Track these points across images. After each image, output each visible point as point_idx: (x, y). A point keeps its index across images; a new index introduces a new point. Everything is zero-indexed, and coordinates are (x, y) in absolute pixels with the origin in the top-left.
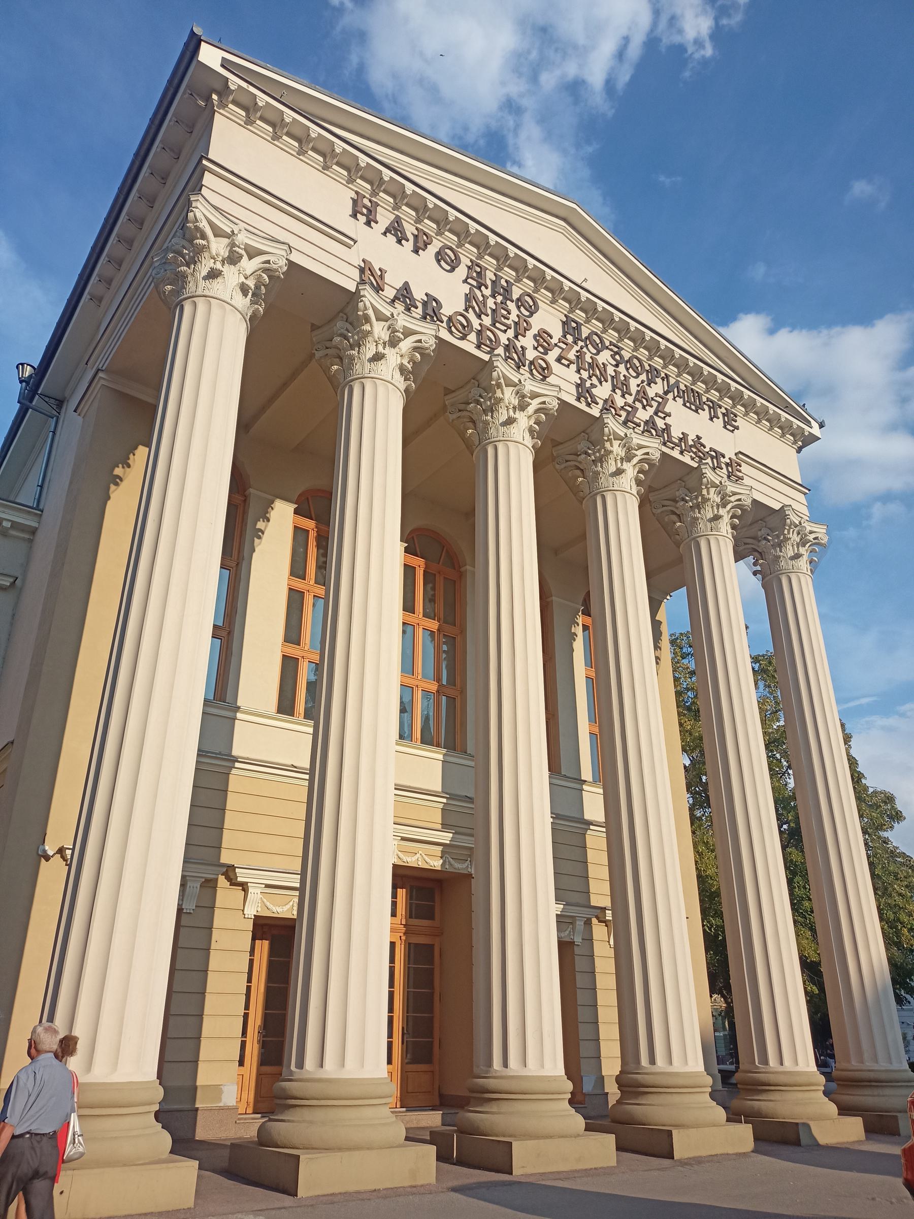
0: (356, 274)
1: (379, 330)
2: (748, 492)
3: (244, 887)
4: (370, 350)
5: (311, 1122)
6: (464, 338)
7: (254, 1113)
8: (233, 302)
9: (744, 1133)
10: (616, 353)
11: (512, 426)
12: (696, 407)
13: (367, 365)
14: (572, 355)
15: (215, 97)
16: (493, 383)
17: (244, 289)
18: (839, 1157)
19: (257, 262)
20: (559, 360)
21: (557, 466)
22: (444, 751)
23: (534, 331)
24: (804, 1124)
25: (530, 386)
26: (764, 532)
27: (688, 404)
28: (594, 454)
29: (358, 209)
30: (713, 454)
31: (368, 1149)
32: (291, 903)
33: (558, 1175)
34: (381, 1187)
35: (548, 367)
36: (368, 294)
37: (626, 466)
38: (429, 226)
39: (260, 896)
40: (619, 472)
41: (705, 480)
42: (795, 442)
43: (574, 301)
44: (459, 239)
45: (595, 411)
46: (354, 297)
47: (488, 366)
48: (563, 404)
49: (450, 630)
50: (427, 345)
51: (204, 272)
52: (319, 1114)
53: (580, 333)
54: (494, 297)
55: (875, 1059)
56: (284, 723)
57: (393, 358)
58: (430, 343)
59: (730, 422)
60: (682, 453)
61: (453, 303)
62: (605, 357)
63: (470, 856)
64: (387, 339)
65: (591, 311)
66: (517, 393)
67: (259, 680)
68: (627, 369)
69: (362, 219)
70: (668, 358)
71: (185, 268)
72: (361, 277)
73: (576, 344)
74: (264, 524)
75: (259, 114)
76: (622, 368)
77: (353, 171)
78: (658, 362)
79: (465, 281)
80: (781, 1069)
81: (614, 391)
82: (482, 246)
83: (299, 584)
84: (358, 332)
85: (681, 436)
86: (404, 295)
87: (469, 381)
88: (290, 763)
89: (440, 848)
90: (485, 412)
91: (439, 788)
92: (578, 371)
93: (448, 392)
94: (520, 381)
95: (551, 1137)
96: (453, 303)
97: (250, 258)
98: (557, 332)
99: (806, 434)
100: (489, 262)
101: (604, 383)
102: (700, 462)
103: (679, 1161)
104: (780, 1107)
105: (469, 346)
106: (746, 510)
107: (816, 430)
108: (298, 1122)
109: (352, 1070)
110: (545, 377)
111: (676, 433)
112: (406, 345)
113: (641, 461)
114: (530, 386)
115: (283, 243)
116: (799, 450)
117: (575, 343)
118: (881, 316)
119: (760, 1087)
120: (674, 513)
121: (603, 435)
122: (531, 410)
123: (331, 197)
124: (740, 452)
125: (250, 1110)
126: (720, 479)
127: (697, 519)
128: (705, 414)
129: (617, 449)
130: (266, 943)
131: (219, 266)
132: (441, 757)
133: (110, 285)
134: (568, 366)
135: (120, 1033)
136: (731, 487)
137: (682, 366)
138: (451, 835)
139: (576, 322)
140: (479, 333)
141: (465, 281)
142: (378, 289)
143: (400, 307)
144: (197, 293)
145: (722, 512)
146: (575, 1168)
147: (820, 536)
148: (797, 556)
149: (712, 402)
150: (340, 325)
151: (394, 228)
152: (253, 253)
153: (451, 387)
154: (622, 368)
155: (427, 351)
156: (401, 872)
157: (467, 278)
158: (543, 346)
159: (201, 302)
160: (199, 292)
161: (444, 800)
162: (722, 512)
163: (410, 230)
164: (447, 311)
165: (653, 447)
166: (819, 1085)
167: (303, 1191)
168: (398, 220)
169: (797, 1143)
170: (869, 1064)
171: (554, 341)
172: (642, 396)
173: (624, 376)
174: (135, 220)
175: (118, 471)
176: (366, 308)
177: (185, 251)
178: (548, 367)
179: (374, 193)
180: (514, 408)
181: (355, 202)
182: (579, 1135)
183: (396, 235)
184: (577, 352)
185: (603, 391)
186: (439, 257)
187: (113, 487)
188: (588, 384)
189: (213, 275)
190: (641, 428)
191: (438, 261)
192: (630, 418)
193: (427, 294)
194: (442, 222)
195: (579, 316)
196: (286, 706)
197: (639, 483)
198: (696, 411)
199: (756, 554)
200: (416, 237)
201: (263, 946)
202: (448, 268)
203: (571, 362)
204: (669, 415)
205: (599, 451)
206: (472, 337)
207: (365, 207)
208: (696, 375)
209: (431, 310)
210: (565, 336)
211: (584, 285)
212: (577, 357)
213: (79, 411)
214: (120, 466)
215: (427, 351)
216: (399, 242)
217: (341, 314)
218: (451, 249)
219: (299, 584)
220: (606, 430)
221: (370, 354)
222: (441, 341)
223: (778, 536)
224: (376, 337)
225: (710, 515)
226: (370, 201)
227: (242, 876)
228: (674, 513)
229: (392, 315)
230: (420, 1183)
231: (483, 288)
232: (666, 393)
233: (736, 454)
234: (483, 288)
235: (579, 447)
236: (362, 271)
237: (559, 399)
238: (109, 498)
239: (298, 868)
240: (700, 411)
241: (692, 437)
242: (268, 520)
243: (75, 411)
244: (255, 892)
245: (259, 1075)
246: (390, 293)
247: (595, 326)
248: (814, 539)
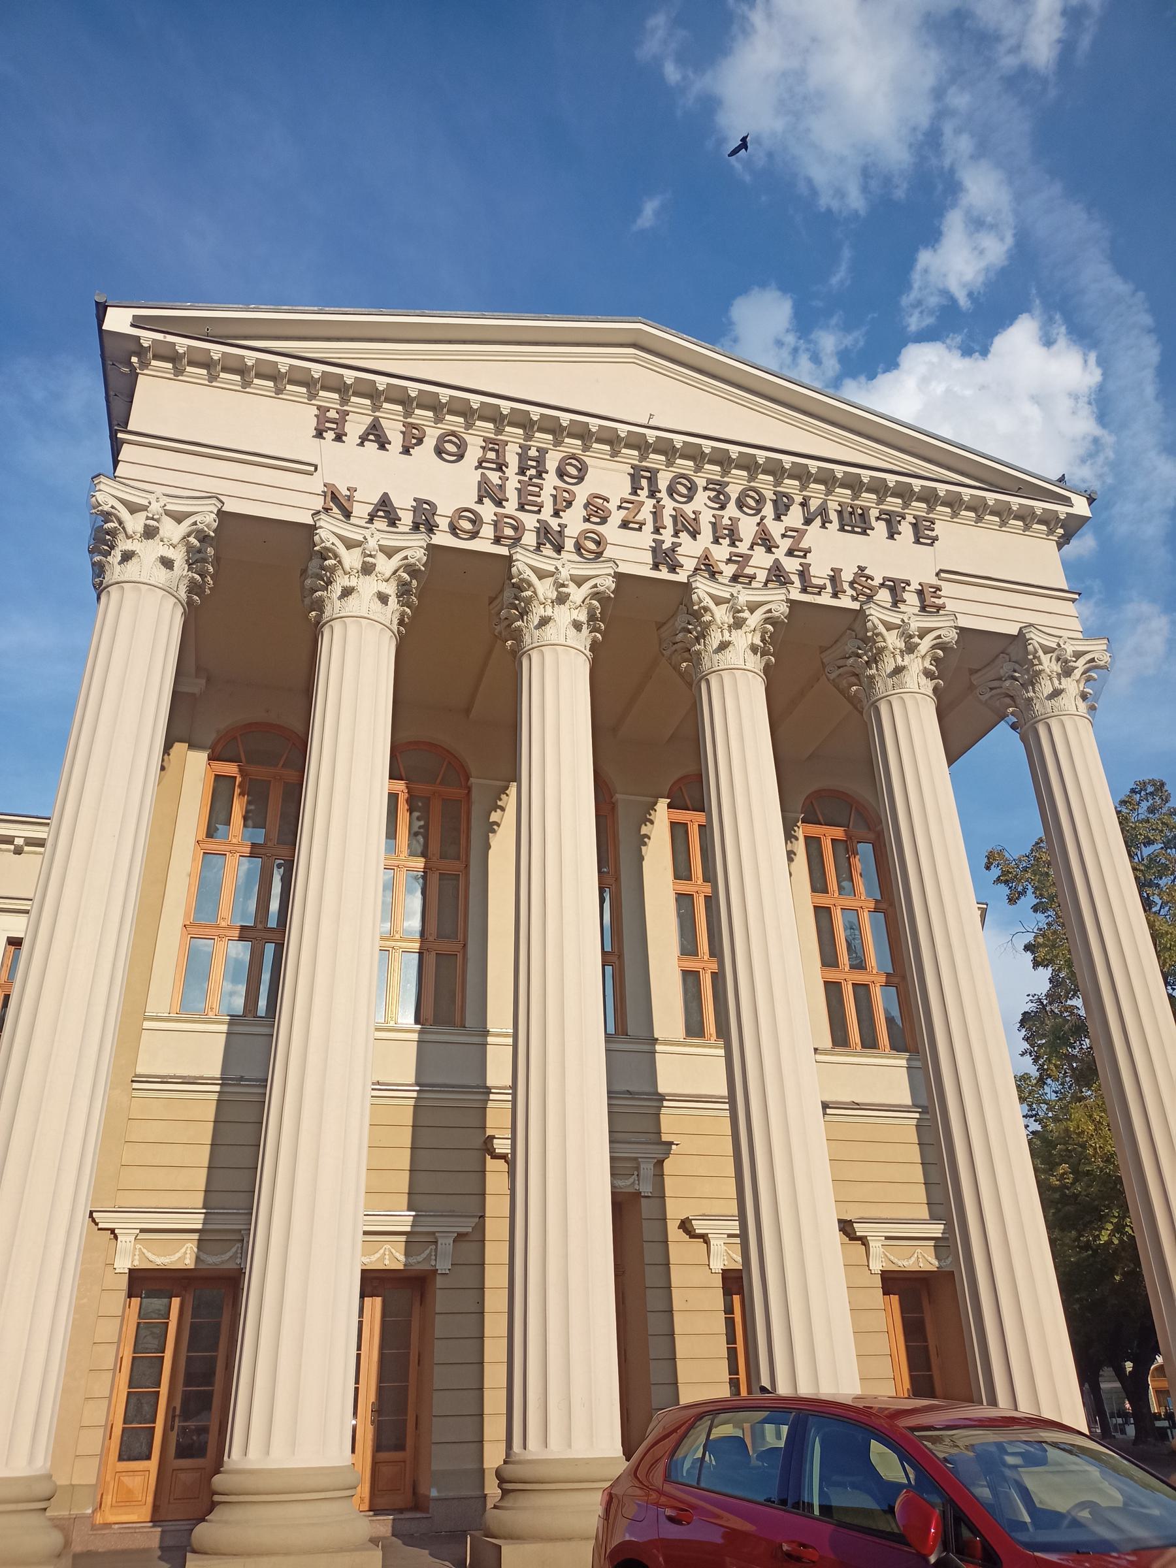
3: (705, 1238)
4: (715, 638)
6: (474, 535)
8: (922, 691)
10: (719, 493)
15: (134, 359)
19: (759, 614)
32: (382, 1251)
58: (782, 610)
59: (923, 534)
64: (731, 621)
66: (1058, 659)
67: (668, 1014)
69: (330, 435)
75: (383, 398)
77: (310, 385)
90: (697, 639)
91: (907, 1100)
94: (903, 621)
109: (581, 1450)
116: (1060, 546)
121: (1028, 653)
123: (284, 422)
124: (942, 571)
130: (378, 1301)
132: (904, 1063)
134: (640, 529)
143: (548, 550)
161: (917, 1115)
189: (724, 646)
198: (864, 533)
201: (375, 1305)
211: (652, 423)
221: (889, 669)
222: (793, 603)
223: (1027, 671)
227: (699, 1227)
237: (956, 628)
239: (735, 1211)
244: (875, 1246)
245: (375, 1464)
247: (571, 446)
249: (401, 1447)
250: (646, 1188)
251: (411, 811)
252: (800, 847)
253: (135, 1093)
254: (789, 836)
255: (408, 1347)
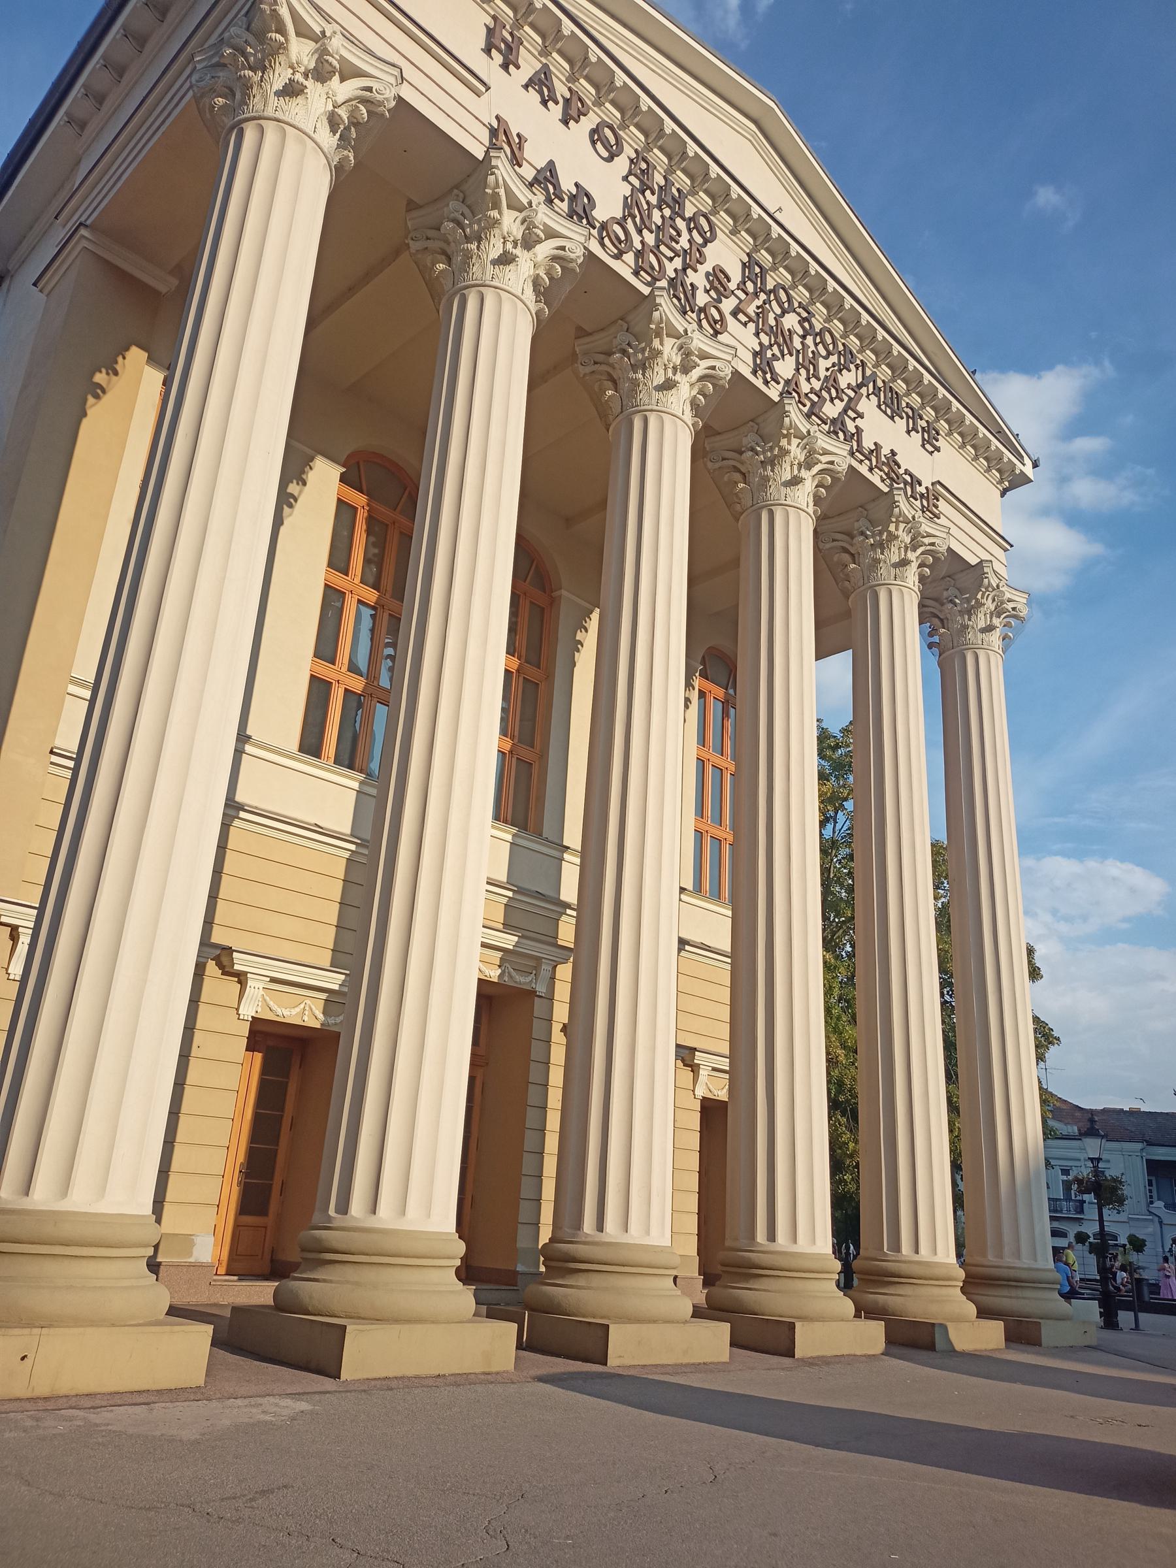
0: (485, 136)
1: (510, 222)
2: (944, 535)
3: (241, 978)
4: (495, 249)
5: (357, 1284)
6: (618, 256)
7: (227, 1274)
9: (873, 1334)
11: (671, 392)
12: (893, 411)
13: (490, 267)
14: (751, 310)
16: (653, 326)
17: (333, 121)
18: (976, 1363)
19: (351, 88)
20: (734, 314)
21: (710, 465)
22: (514, 830)
23: (707, 267)
24: (941, 1325)
25: (699, 341)
26: (952, 591)
27: (883, 407)
28: (764, 452)
29: (496, 41)
30: (908, 478)
31: (433, 1322)
32: (302, 1006)
33: (679, 1368)
34: (446, 1372)
35: (722, 320)
36: (502, 166)
37: (804, 474)
38: (586, 89)
39: (262, 992)
40: (795, 481)
41: (896, 510)
42: (1001, 482)
43: (761, 236)
44: (623, 117)
45: (773, 392)
46: (484, 166)
47: (649, 302)
48: (736, 374)
49: (533, 673)
50: (572, 256)
51: (278, 85)
52: (369, 1274)
53: (763, 282)
54: (661, 210)
55: (1018, 1254)
56: (307, 766)
57: (526, 266)
58: (578, 254)
59: (930, 440)
60: (871, 470)
61: (607, 208)
62: (791, 321)
63: (535, 968)
64: (519, 237)
65: (781, 254)
66: (680, 348)
68: (816, 345)
70: (868, 339)
71: (251, 73)
72: (491, 141)
73: (758, 297)
74: (298, 488)
76: (809, 340)
78: (854, 342)
79: (625, 178)
80: (916, 1258)
81: (797, 370)
82: (653, 133)
83: (339, 581)
84: (480, 220)
85: (873, 447)
86: (547, 178)
87: (615, 322)
88: (313, 822)
89: (499, 954)
90: (634, 368)
92: (757, 334)
93: (581, 333)
95: (655, 1322)
96: (607, 208)
97: (342, 80)
98: (736, 276)
99: (1018, 472)
100: (658, 157)
101: (787, 357)
102: (891, 486)
103: (802, 1360)
104: (915, 1303)
105: (624, 268)
106: (939, 559)
107: (1028, 470)
108: (338, 1282)
110: (717, 333)
111: (868, 444)
112: (545, 249)
113: (822, 471)
114: (699, 341)
115: (394, 65)
116: (1003, 494)
117: (756, 295)
118: (1050, 367)
119: (885, 1278)
120: (846, 551)
122: (696, 373)
124: (939, 482)
125: (222, 1270)
126: (913, 512)
127: (879, 561)
128: (901, 424)
129: (796, 450)
131: (299, 77)
132: (509, 838)
133: (101, 103)
134: (745, 324)
135: (111, 1147)
136: (926, 527)
137: (882, 354)
138: (516, 939)
139: (760, 267)
140: (639, 254)
141: (625, 178)
142: (516, 161)
144: (266, 114)
145: (911, 556)
146: (680, 1361)
147: (1019, 606)
148: (989, 629)
149: (912, 409)
150: (454, 206)
151: (540, 80)
152: (348, 72)
153: (587, 327)
154: (809, 340)
155: (571, 265)
156: (260, 1028)
157: (630, 173)
158: (716, 290)
159: (270, 128)
160: (269, 112)
161: (510, 894)
162: (911, 556)
163: (561, 90)
164: (601, 214)
165: (838, 453)
166: (955, 1280)
167: (348, 1372)
168: (546, 71)
169: (931, 1347)
170: (1009, 1260)
171: (732, 286)
172: (831, 382)
173: (813, 352)
174: (155, 6)
175: (100, 378)
176: (497, 185)
177: (249, 50)
178: (722, 318)
179: (517, 25)
180: (675, 368)
181: (490, 32)
182: (686, 1322)
183: (541, 93)
184: (758, 308)
185: (785, 368)
186: (596, 136)
187: (91, 400)
188: (769, 354)
189: (292, 90)
190: (826, 427)
191: (593, 143)
192: (816, 410)
193: (577, 185)
194: (604, 87)
195: (765, 257)
196: (311, 745)
197: (817, 500)
198: (892, 418)
199: (936, 621)
200: (567, 101)
202: (605, 154)
203: (751, 320)
204: (861, 416)
205: (771, 449)
206: (629, 257)
207: (504, 40)
208: (898, 369)
209: (580, 206)
210: (744, 283)
211: (777, 215)
212: (757, 314)
213: (40, 285)
214: (104, 370)
215: (571, 265)
216: (544, 103)
217: (456, 191)
218: (611, 128)
219: (339, 581)
220: (787, 420)
222: (590, 256)
223: (968, 601)
224: (505, 230)
225: (895, 558)
226: (511, 34)
227: (241, 963)
228: (846, 551)
229: (530, 203)
230: (494, 1370)
231: (648, 193)
232: (860, 386)
233: (933, 484)
234: (648, 193)
235: (745, 441)
236: (494, 133)
238: (85, 415)
240: (897, 418)
241: (885, 451)
242: (305, 484)
243: (35, 284)
244: (255, 986)
246: (529, 173)
247: (781, 276)
248: (1014, 609)
249: (263, 1211)
250: (541, 989)
251: (369, 532)
252: (694, 696)
253: (52, 769)
254: (689, 685)
255: (282, 1109)
